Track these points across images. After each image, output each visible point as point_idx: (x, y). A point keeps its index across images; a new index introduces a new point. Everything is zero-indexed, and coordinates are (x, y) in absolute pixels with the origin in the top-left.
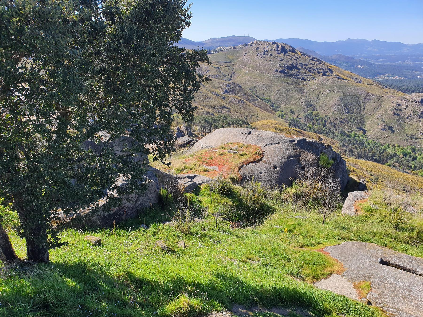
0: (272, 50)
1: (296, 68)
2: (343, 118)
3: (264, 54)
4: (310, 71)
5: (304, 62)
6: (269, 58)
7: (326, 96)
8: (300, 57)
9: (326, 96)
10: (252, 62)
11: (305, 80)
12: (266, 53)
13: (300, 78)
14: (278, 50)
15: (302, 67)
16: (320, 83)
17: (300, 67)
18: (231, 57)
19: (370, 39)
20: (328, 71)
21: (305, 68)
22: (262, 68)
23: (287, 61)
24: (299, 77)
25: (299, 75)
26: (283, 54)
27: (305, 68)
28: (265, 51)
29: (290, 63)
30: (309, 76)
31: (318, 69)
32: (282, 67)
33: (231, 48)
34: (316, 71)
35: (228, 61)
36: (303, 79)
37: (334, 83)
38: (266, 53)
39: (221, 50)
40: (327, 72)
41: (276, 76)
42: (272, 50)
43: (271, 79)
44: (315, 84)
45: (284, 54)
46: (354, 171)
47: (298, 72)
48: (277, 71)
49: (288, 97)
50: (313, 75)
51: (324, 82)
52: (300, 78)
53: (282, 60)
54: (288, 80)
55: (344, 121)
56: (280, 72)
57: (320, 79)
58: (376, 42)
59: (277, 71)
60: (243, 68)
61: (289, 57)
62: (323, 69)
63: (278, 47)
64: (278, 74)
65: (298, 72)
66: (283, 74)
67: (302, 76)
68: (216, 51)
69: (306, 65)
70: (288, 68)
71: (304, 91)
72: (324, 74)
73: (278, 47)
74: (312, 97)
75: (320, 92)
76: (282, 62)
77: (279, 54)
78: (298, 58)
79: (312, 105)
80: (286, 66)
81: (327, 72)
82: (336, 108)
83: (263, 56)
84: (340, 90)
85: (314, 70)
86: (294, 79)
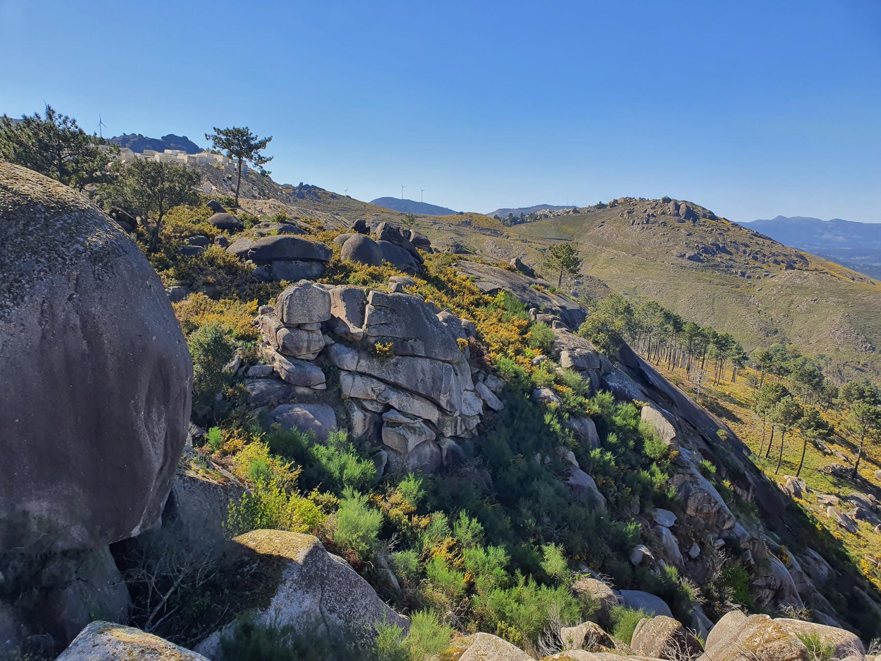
0: (663, 213)
1: (724, 250)
2: (862, 362)
3: (647, 222)
4: (755, 259)
5: (740, 240)
6: (661, 231)
7: (809, 311)
8: (729, 230)
9: (809, 311)
10: (620, 238)
11: (749, 277)
12: (652, 219)
13: (736, 273)
14: (678, 215)
15: (737, 249)
16: (789, 284)
17: (733, 251)
18: (571, 230)
19: (825, 215)
20: (799, 259)
21: (745, 252)
22: (647, 249)
23: (702, 237)
24: (734, 270)
25: (732, 267)
26: (690, 223)
27: (745, 252)
28: (648, 215)
29: (710, 240)
30: (755, 268)
31: (774, 255)
32: (693, 248)
33: (568, 213)
34: (772, 259)
35: (566, 237)
36: (743, 274)
37: (822, 284)
38: (652, 219)
39: (546, 216)
40: (795, 262)
41: (682, 267)
42: (663, 213)
43: (672, 274)
44: (775, 286)
45: (694, 222)
46: (255, 222)
47: (730, 260)
48: (683, 256)
49: (717, 312)
50: (765, 266)
51: (798, 281)
52: (736, 273)
53: (690, 235)
54: (709, 274)
55: (867, 370)
56: (690, 258)
57: (783, 276)
58: (839, 224)
59: (683, 256)
60: (601, 250)
61: (704, 228)
62: (786, 255)
63: (677, 207)
64: (685, 262)
65: (730, 260)
66: (696, 264)
67: (740, 268)
68: (536, 219)
69: (747, 246)
70: (706, 250)
71: (752, 300)
72: (790, 266)
73: (677, 207)
74: (773, 313)
75: (792, 302)
76: (691, 238)
77: (679, 221)
78: (726, 231)
79: (776, 332)
80: (701, 246)
81: (795, 262)
82: (839, 338)
83: (645, 226)
84: (840, 300)
85: (764, 256)
86: (723, 274)
